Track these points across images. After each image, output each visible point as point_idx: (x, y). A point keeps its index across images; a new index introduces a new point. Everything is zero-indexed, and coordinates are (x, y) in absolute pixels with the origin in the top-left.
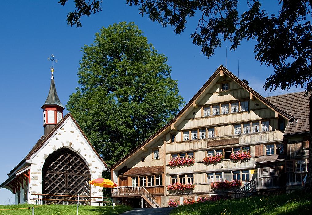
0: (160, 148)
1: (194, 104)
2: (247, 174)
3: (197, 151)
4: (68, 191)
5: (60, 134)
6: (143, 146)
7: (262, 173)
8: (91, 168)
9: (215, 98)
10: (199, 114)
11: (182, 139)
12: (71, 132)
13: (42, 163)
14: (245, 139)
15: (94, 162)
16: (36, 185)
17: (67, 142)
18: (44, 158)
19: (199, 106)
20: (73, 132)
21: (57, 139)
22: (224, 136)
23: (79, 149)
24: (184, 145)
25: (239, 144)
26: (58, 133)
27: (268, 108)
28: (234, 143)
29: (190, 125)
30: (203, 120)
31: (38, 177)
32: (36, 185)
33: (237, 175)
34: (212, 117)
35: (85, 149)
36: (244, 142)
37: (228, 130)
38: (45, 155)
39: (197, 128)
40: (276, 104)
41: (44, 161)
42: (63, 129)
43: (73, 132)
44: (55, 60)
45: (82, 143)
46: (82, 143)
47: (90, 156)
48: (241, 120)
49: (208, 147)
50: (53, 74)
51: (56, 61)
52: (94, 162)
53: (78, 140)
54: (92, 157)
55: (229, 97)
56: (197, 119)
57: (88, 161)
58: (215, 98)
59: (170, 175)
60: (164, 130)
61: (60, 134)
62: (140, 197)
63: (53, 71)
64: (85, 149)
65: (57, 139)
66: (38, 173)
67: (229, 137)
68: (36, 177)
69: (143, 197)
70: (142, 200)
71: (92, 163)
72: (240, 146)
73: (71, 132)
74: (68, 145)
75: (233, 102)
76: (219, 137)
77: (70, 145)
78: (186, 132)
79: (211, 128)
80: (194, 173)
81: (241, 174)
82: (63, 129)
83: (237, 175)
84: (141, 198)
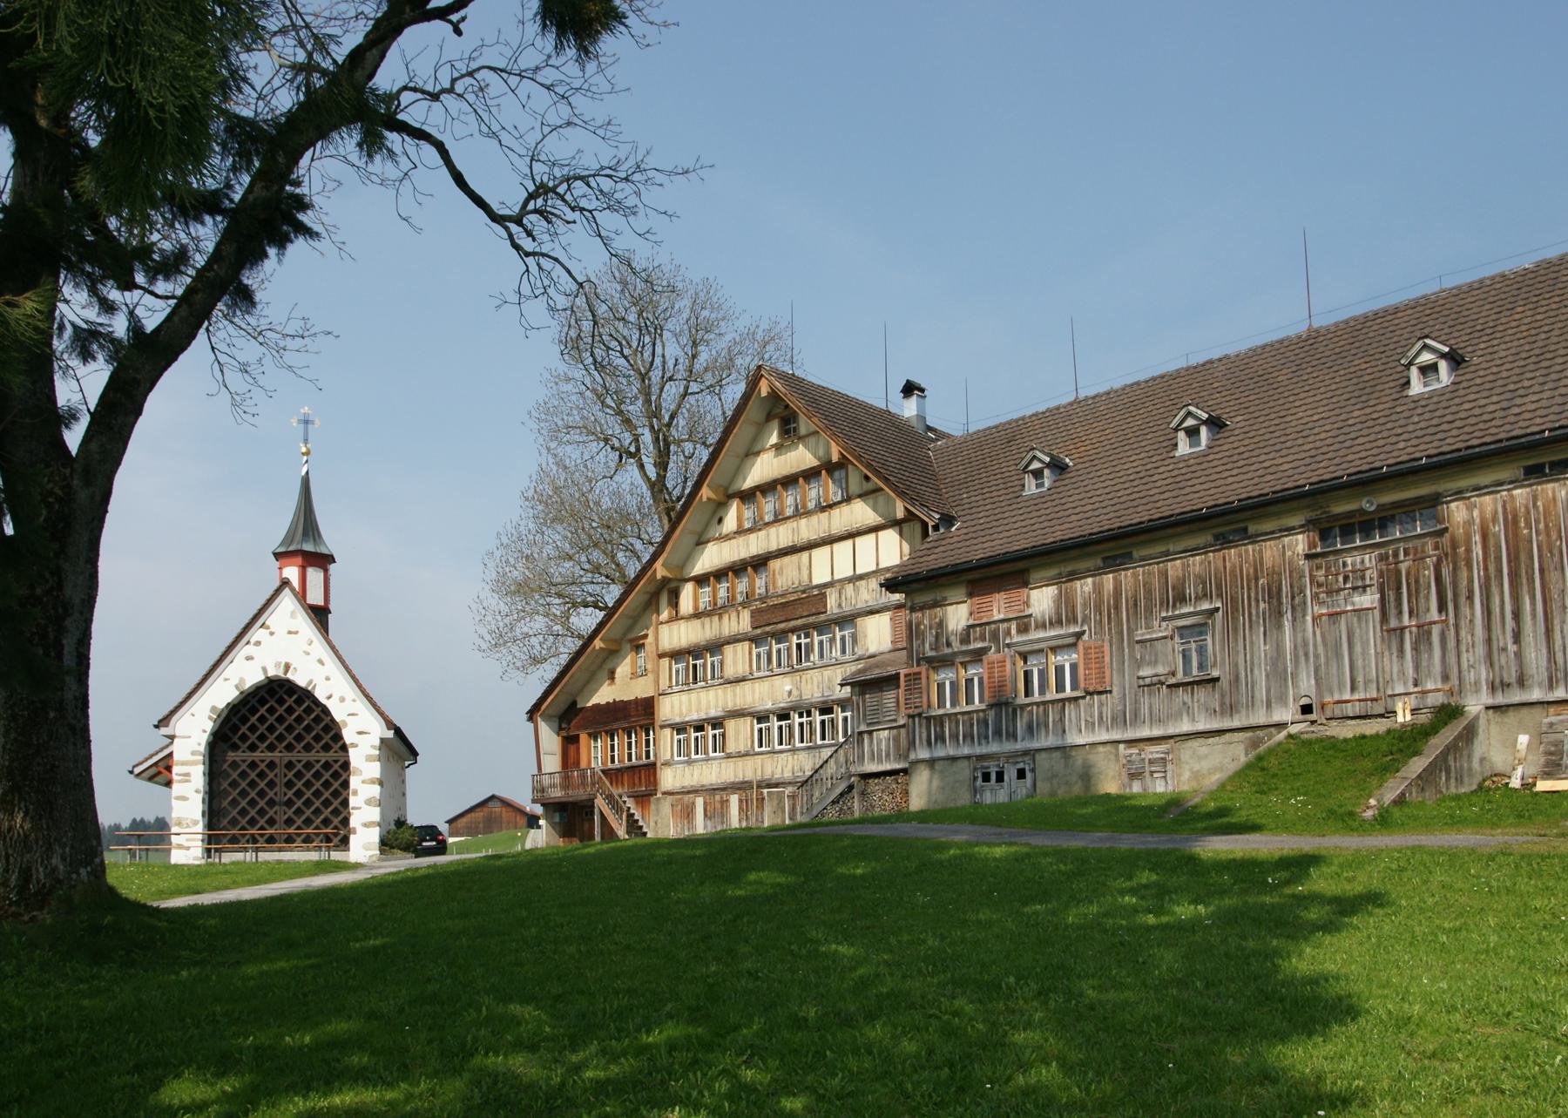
0: (646, 636)
1: (705, 493)
2: (1064, 691)
3: (729, 643)
4: (284, 808)
5: (258, 643)
6: (600, 637)
7: (864, 719)
8: (348, 736)
9: (764, 468)
10: (730, 522)
11: (696, 607)
12: (290, 633)
13: (205, 731)
14: (840, 597)
15: (353, 715)
16: (184, 798)
17: (278, 665)
18: (210, 718)
19: (729, 495)
20: (296, 633)
21: (249, 658)
22: (790, 590)
23: (310, 682)
24: (699, 627)
25: (826, 612)
26: (252, 641)
27: (882, 489)
28: (814, 610)
29: (711, 558)
30: (741, 540)
31: (192, 773)
32: (184, 798)
33: (948, 705)
34: (760, 530)
35: (328, 679)
36: (840, 606)
37: (799, 569)
38: (213, 709)
39: (725, 569)
40: (1058, 450)
41: (209, 726)
42: (268, 628)
43: (296, 633)
44: (313, 422)
45: (321, 662)
46: (321, 662)
47: (342, 700)
48: (829, 531)
49: (754, 628)
50: (307, 461)
51: (317, 422)
52: (353, 715)
53: (308, 654)
54: (348, 700)
55: (801, 457)
56: (727, 537)
57: (338, 713)
58: (764, 468)
59: (670, 726)
60: (642, 583)
61: (258, 643)
62: (590, 804)
63: (307, 453)
64: (328, 679)
65: (249, 658)
66: (194, 763)
67: (804, 592)
68: (187, 775)
69: (600, 802)
70: (596, 810)
71: (349, 720)
72: (828, 620)
73: (290, 633)
74: (281, 674)
75: (810, 475)
76: (780, 593)
77: (286, 671)
78: (701, 580)
79: (759, 563)
80: (724, 718)
81: (818, 718)
82: (268, 628)
83: (948, 705)
84: (594, 807)
